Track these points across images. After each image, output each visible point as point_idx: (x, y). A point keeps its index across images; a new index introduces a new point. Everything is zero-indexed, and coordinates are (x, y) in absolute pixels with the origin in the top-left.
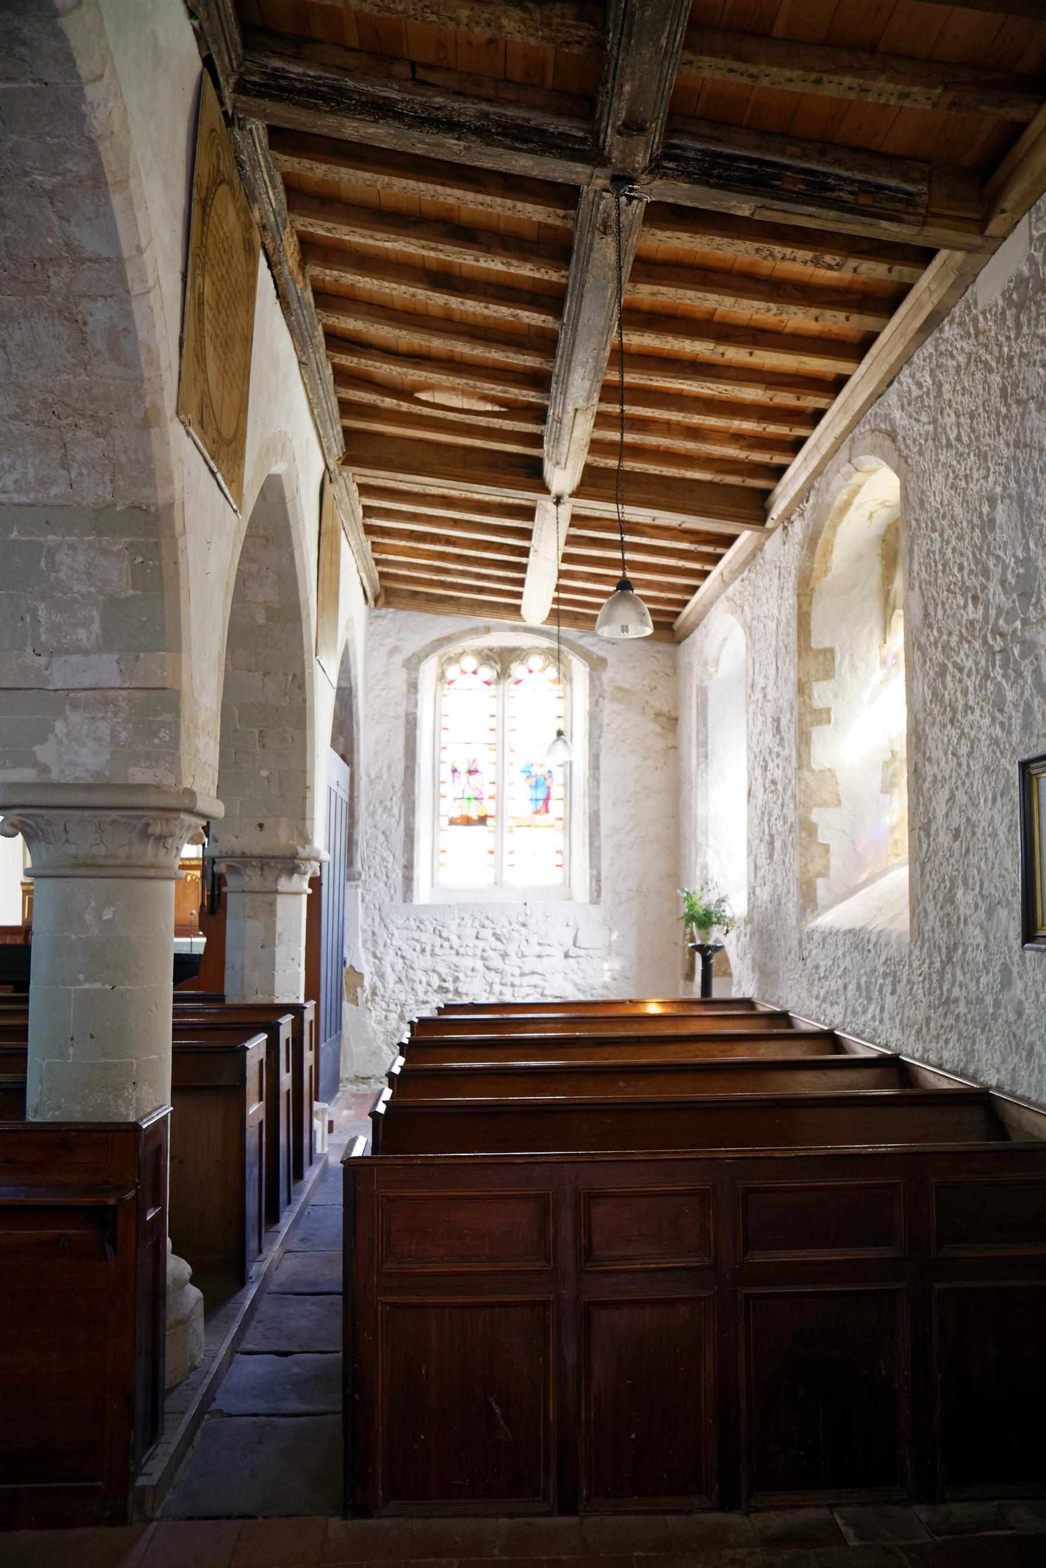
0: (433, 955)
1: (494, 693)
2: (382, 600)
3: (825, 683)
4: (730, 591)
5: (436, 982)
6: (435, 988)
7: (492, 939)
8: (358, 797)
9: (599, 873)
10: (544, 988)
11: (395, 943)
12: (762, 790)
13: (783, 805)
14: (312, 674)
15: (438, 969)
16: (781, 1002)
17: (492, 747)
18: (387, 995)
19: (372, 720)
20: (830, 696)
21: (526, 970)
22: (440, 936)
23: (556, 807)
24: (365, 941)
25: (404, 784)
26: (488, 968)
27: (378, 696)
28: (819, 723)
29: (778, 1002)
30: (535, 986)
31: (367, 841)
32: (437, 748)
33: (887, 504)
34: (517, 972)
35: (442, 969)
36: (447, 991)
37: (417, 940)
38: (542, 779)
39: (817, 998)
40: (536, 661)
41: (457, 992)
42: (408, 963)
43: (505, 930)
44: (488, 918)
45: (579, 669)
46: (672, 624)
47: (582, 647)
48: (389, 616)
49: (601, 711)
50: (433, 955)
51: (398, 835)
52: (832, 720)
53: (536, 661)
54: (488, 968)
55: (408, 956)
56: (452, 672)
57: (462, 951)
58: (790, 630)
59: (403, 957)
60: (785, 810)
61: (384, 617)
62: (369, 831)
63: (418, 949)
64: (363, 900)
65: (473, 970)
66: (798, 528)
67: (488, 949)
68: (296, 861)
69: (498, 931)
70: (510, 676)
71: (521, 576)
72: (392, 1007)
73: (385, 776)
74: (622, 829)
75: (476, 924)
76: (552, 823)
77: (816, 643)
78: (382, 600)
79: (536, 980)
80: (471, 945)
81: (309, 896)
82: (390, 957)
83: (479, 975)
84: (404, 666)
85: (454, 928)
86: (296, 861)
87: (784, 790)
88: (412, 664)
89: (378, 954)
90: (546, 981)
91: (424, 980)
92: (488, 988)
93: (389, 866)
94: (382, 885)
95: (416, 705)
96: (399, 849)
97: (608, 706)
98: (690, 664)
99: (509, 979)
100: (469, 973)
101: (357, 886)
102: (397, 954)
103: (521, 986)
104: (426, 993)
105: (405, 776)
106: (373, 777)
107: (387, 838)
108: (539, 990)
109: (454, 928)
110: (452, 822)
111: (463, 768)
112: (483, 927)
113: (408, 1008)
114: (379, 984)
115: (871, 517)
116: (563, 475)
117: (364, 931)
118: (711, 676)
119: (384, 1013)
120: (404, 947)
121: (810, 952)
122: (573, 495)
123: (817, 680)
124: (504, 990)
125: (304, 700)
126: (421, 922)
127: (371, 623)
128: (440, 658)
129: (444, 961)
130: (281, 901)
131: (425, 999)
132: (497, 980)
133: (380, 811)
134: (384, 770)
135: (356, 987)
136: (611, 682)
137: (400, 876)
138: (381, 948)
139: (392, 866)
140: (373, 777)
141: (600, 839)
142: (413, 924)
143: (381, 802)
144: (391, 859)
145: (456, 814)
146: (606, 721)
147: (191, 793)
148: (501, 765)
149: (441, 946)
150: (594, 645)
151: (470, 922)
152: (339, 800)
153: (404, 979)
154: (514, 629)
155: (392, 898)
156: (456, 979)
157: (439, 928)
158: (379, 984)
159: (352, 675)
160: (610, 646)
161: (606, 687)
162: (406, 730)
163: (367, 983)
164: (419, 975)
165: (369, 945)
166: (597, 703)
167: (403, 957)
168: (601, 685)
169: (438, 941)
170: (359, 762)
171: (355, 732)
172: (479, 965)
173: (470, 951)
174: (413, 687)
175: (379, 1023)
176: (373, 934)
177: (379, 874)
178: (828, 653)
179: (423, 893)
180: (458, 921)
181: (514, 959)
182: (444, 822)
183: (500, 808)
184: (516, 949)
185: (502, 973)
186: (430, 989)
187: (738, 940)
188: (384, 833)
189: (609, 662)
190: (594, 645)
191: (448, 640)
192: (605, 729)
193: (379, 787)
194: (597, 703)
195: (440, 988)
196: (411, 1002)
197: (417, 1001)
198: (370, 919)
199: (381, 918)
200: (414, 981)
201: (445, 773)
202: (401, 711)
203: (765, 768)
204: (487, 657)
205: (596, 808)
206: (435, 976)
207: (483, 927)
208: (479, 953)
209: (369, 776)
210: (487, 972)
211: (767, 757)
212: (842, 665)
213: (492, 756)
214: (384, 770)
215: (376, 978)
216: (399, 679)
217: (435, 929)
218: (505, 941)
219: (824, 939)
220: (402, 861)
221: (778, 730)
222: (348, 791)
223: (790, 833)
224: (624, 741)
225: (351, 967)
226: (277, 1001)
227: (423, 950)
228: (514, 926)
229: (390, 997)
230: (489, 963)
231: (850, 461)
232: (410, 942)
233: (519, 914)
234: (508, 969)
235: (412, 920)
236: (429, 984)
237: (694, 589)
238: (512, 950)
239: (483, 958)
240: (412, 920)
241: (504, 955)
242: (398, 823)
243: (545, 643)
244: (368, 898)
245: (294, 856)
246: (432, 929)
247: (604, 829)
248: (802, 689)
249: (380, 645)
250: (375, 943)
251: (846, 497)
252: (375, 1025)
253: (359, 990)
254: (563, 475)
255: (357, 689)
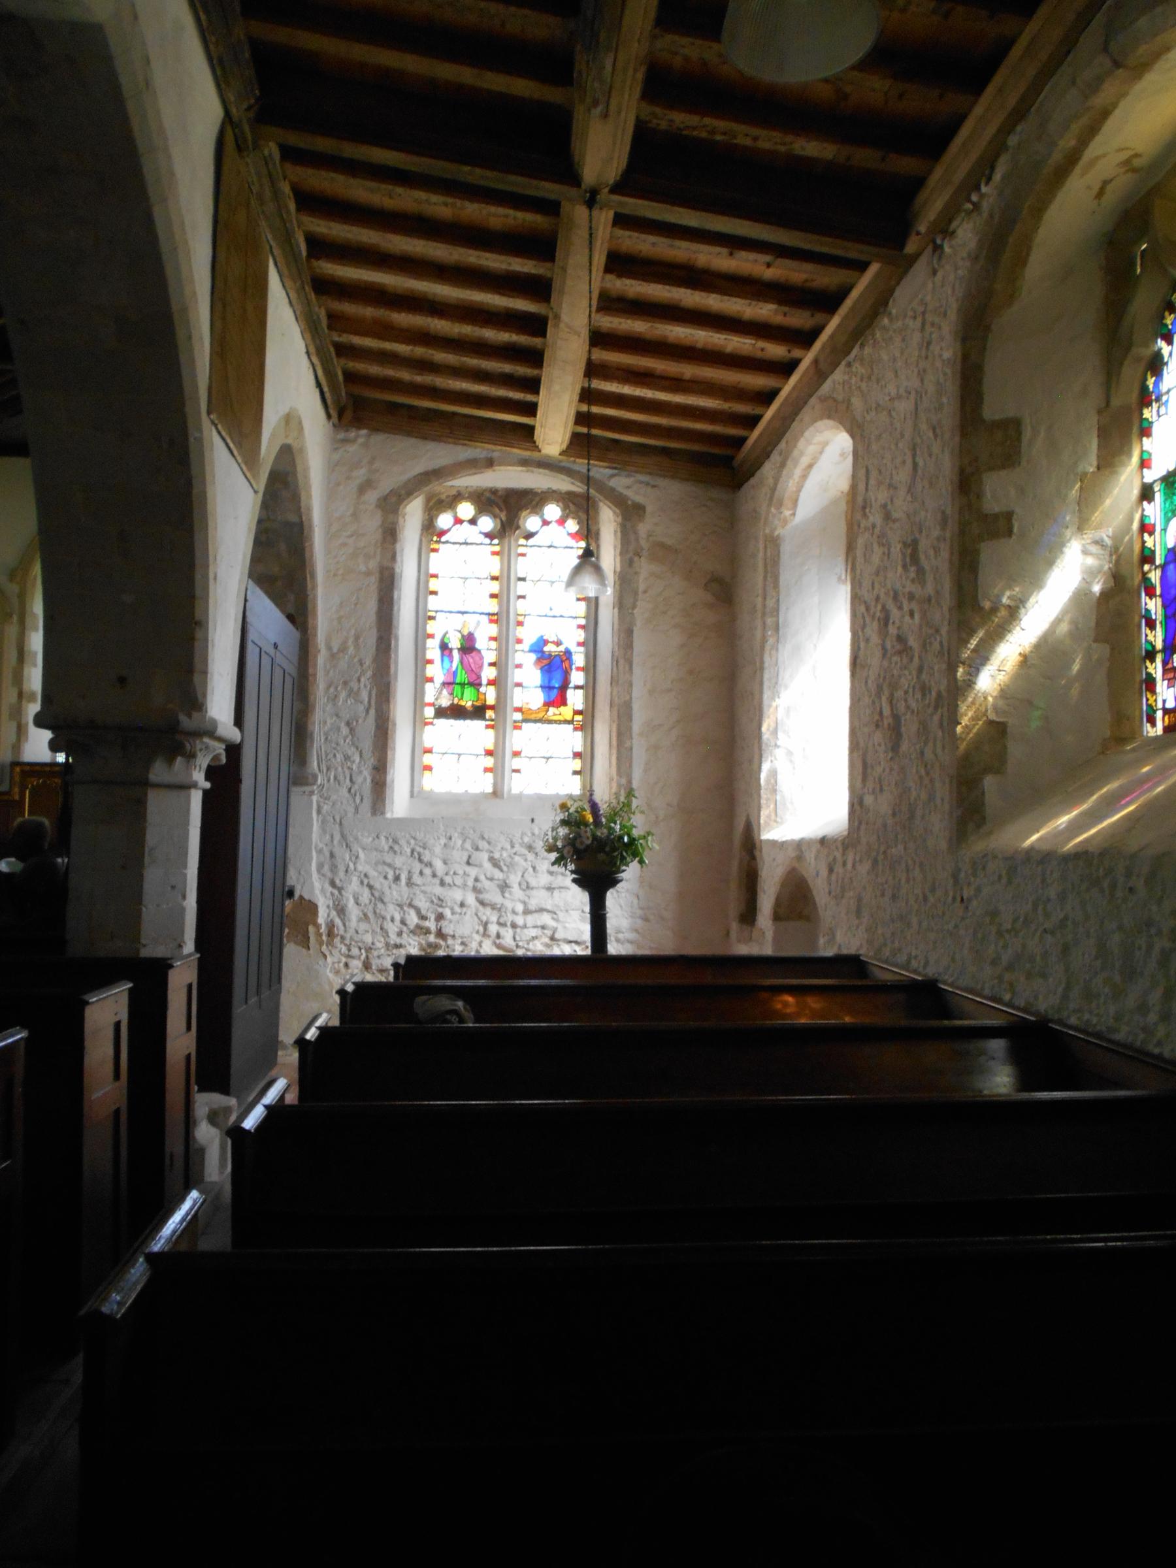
0: (410, 883)
1: (497, 549)
2: (349, 414)
3: (1003, 473)
4: (826, 387)
5: (413, 919)
6: (412, 927)
7: (487, 865)
8: (315, 675)
9: (630, 782)
10: (555, 930)
11: (360, 868)
12: (878, 653)
13: (920, 670)
14: (200, 441)
15: (416, 903)
16: (914, 964)
17: (494, 618)
18: (348, 936)
19: (335, 575)
20: (1013, 492)
21: (532, 907)
22: (420, 860)
23: (576, 699)
24: (320, 867)
25: (376, 659)
26: (482, 903)
27: (345, 545)
28: (994, 535)
29: (909, 961)
30: (543, 927)
31: (326, 734)
32: (423, 617)
33: (1137, 163)
34: (520, 908)
35: (422, 903)
36: (428, 931)
37: (389, 865)
38: (558, 660)
39: (994, 962)
40: (553, 511)
41: (440, 934)
42: (377, 894)
43: (505, 854)
44: (483, 838)
45: (608, 520)
46: (732, 458)
47: (613, 490)
48: (361, 440)
49: (636, 573)
50: (410, 883)
51: (368, 726)
52: (1015, 530)
53: (553, 511)
54: (482, 903)
55: (377, 886)
56: (444, 520)
57: (448, 879)
58: (945, 400)
59: (370, 887)
60: (924, 676)
61: (354, 441)
62: (329, 722)
63: (391, 876)
64: (319, 812)
65: (462, 905)
66: (966, 235)
67: (482, 878)
68: (178, 737)
69: (497, 855)
70: (518, 527)
71: (530, 398)
72: (355, 951)
73: (351, 650)
74: (660, 725)
75: (468, 845)
76: (569, 718)
77: (991, 411)
78: (349, 414)
79: (546, 919)
80: (461, 872)
81: (206, 793)
82: (354, 885)
83: (470, 912)
84: (378, 506)
85: (438, 850)
86: (178, 737)
87: (924, 646)
88: (392, 504)
89: (337, 882)
90: (557, 920)
91: (398, 917)
92: (481, 929)
93: (354, 767)
94: (344, 791)
95: (393, 558)
96: (367, 744)
97: (645, 568)
98: (755, 511)
99: (510, 918)
100: (457, 909)
101: (312, 793)
102: (362, 883)
103: (525, 926)
104: (400, 934)
105: (377, 650)
106: (335, 650)
107: (352, 730)
108: (549, 933)
109: (438, 850)
110: (441, 713)
111: (455, 643)
112: (477, 849)
113: (376, 953)
114: (338, 921)
115: (1100, 194)
116: (602, 151)
117: (320, 852)
118: (785, 522)
119: (344, 960)
120: (373, 873)
121: (978, 890)
122: (617, 189)
123: (991, 469)
124: (503, 931)
125: (189, 484)
126: (395, 841)
127: (336, 449)
128: (428, 500)
129: (424, 892)
130: (155, 802)
131: (398, 941)
132: (494, 919)
133: (343, 695)
134: (350, 642)
135: (307, 925)
136: (649, 536)
137: (369, 780)
138: (342, 874)
139: (359, 767)
140: (335, 650)
141: (631, 738)
142: (384, 844)
143: (345, 683)
144: (357, 759)
145: (445, 702)
146: (642, 587)
147: (214, 723)
148: (502, 641)
149: (421, 873)
150: (628, 487)
151: (460, 842)
152: (278, 672)
153: (371, 915)
154: (524, 463)
155: (357, 809)
156: (440, 917)
157: (418, 849)
158: (338, 921)
159: (303, 504)
160: (649, 490)
161: (643, 543)
162: (380, 590)
163: (321, 920)
164: (392, 911)
165: (326, 869)
166: (631, 563)
167: (370, 887)
168: (637, 540)
169: (417, 867)
170: (315, 628)
171: (309, 586)
172: (471, 899)
173: (459, 881)
174: (391, 534)
175: (337, 972)
176: (332, 855)
177: (341, 778)
178: (1011, 429)
179: (399, 804)
180: (443, 841)
181: (517, 892)
182: (429, 712)
183: (502, 697)
184: (519, 878)
185: (499, 910)
186: (405, 929)
187: (831, 871)
188: (348, 724)
189: (649, 509)
190: (628, 487)
191: (436, 474)
192: (640, 596)
193: (343, 664)
194: (631, 563)
195: (418, 927)
196: (379, 945)
197: (387, 945)
198: (328, 837)
199: (343, 836)
200: (384, 918)
201: (433, 650)
202: (373, 564)
203: (885, 621)
204: (486, 501)
205: (628, 698)
206: (412, 913)
207: (477, 849)
208: (470, 883)
209: (329, 648)
210: (481, 908)
211: (891, 605)
212: (1034, 445)
213: (493, 630)
214: (350, 642)
215: (334, 913)
216: (372, 523)
217: (413, 851)
218: (505, 868)
219: (1012, 871)
220: (371, 761)
221: (914, 558)
222: (295, 660)
223: (936, 708)
224: (665, 613)
225: (301, 897)
226: (145, 953)
227: (397, 878)
228: (517, 848)
229: (351, 939)
230: (486, 897)
231: (1105, 49)
232: (380, 868)
233: (523, 834)
234: (509, 905)
235: (383, 838)
236: (403, 922)
237: (767, 397)
238: (514, 880)
239: (475, 889)
240: (383, 838)
241: (504, 887)
242: (367, 711)
243: (563, 484)
244: (326, 808)
245: (173, 728)
246: (409, 851)
247: (637, 726)
248: (966, 484)
249: (348, 478)
250: (334, 868)
251: (1073, 143)
252: (331, 976)
253: (311, 929)
254: (602, 151)
255: (311, 527)
